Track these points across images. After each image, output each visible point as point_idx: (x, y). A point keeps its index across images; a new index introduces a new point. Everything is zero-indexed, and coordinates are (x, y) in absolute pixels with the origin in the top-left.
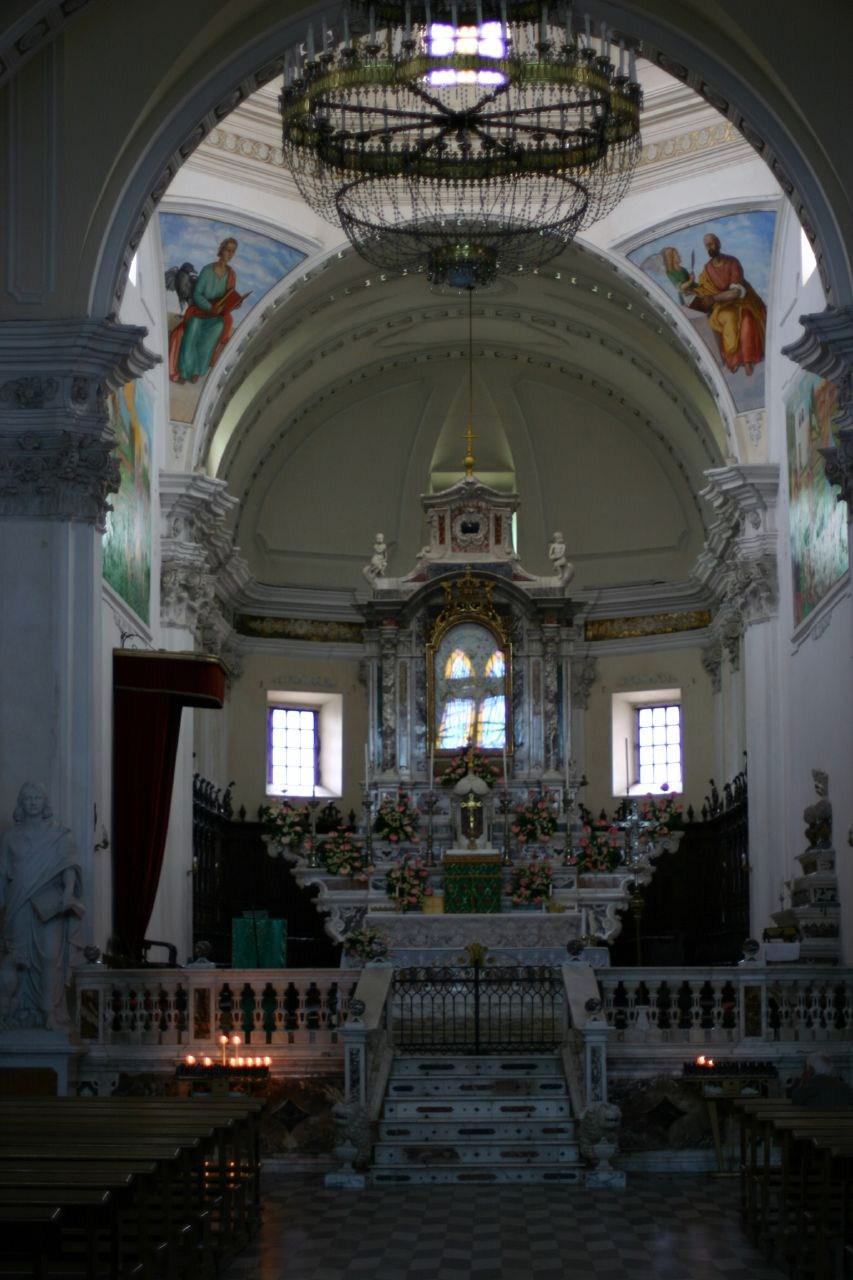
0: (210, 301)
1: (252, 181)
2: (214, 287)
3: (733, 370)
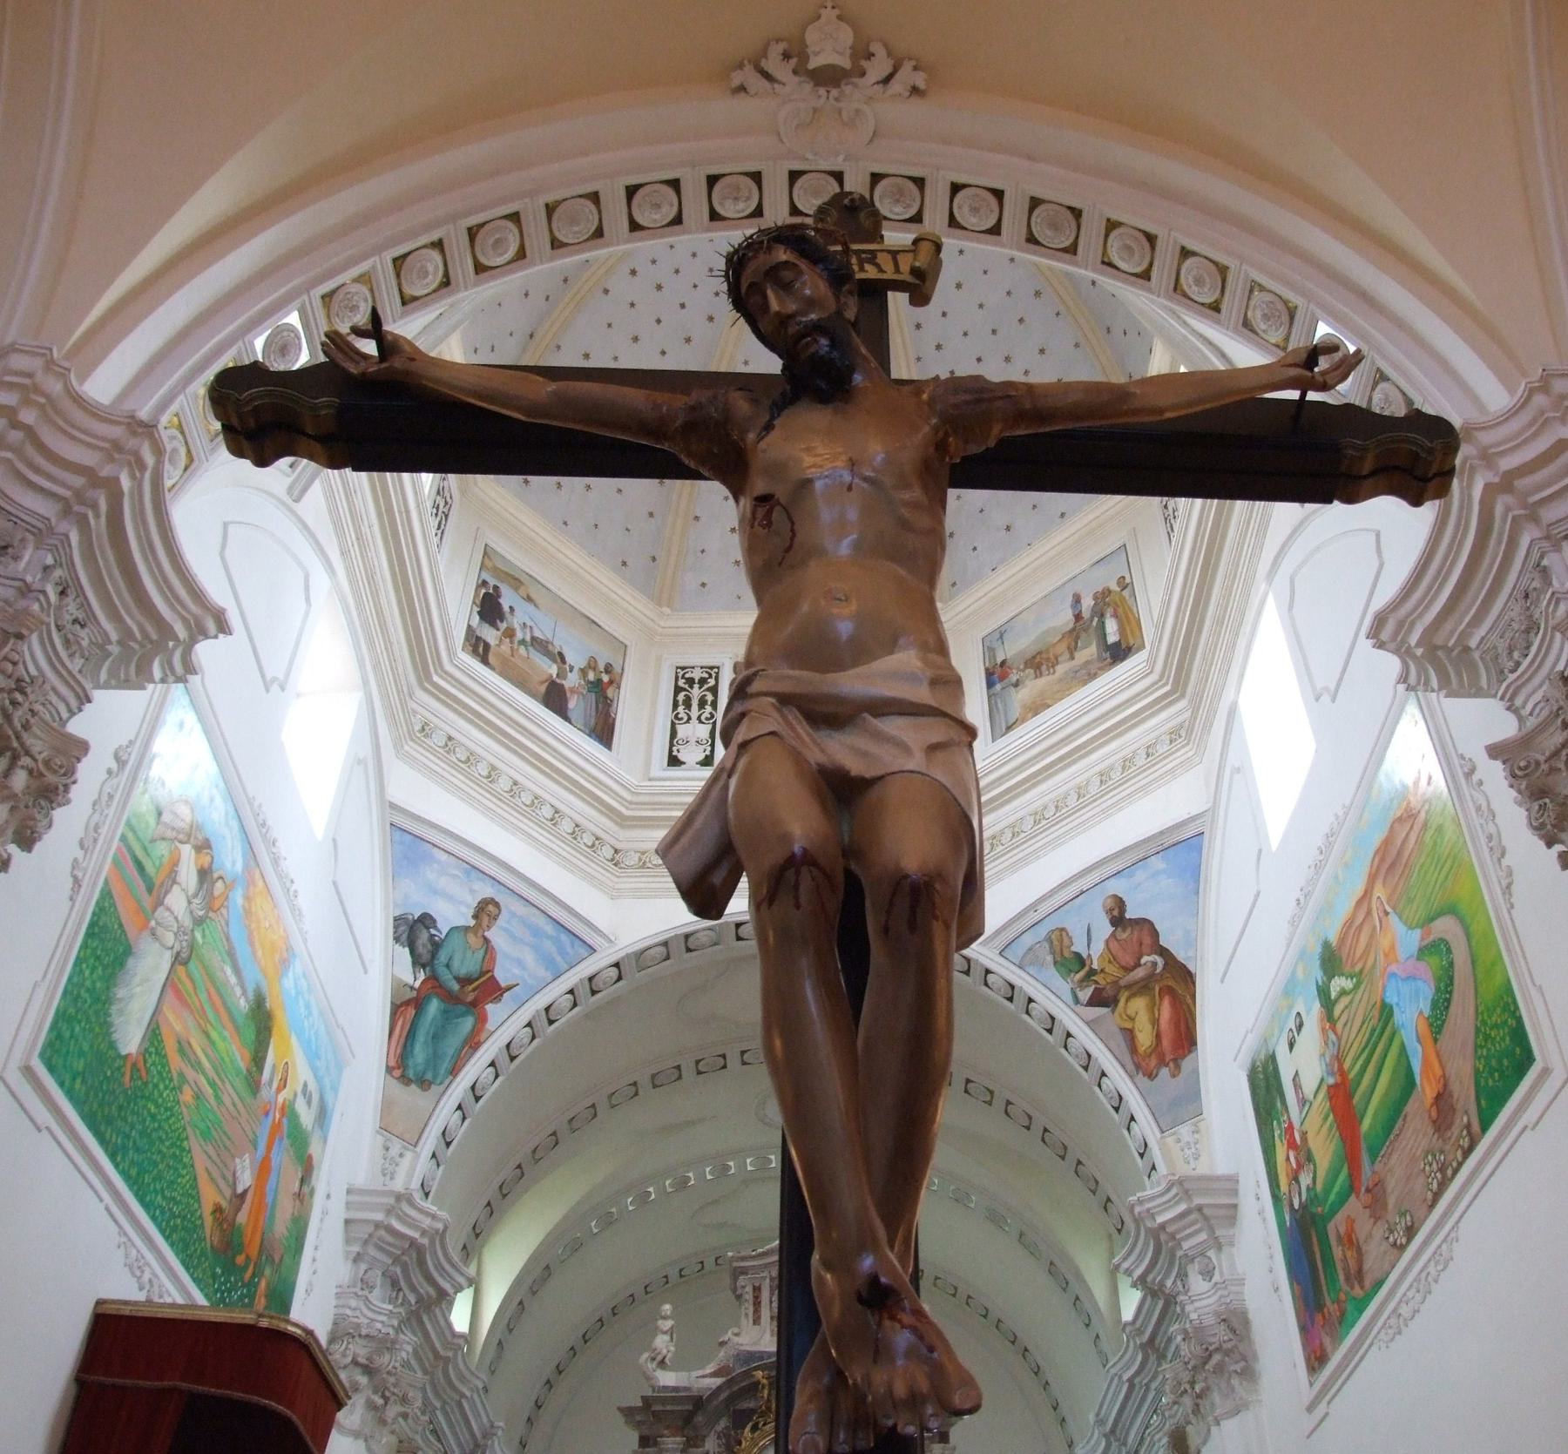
0: (458, 979)
1: (530, 836)
2: (466, 962)
3: (1151, 1076)
